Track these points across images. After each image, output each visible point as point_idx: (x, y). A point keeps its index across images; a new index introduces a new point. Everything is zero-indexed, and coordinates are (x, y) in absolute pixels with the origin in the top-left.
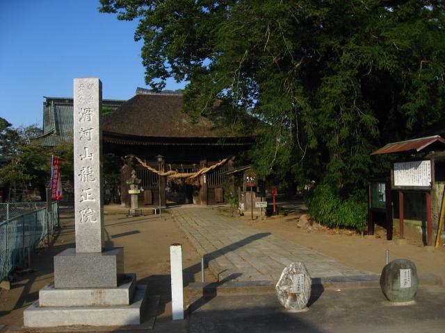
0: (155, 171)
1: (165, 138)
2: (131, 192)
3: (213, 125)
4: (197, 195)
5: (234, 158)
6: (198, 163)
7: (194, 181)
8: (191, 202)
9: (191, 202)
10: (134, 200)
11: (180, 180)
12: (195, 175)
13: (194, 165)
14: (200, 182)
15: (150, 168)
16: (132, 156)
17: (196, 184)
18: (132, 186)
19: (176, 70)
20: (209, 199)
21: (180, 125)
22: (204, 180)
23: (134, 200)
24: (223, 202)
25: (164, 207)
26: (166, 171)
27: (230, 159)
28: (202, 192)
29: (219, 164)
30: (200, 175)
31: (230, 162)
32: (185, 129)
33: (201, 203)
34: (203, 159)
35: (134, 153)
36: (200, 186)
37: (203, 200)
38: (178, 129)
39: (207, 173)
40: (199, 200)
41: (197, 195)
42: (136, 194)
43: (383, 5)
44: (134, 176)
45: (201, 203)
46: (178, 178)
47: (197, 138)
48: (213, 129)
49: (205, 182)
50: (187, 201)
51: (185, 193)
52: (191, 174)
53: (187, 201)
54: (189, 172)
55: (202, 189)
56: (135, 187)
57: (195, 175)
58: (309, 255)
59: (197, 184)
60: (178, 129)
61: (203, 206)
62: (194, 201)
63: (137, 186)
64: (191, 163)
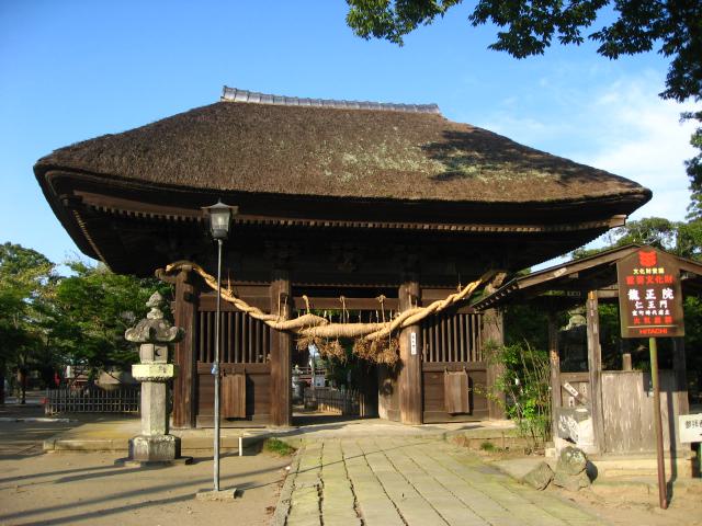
0: (257, 314)
1: (284, 195)
2: (139, 371)
3: (441, 168)
4: (390, 391)
5: (503, 276)
6: (393, 294)
7: (380, 349)
8: (374, 415)
9: (374, 415)
10: (151, 400)
11: (336, 345)
12: (385, 328)
13: (382, 297)
14: (398, 352)
15: (241, 306)
16: (186, 266)
17: (387, 357)
18: (146, 350)
19: (353, 381)
20: (427, 405)
21: (336, 166)
22: (409, 345)
23: (151, 400)
24: (470, 414)
25: (285, 428)
26: (293, 316)
27: (491, 280)
28: (406, 383)
29: (457, 297)
30: (399, 330)
31: (490, 289)
32: (350, 175)
33: (403, 415)
34: (408, 280)
35: (191, 259)
36: (399, 364)
37: (409, 405)
38: (328, 174)
39: (422, 324)
40: (394, 405)
41: (390, 391)
42: (156, 380)
43: (694, 31)
44: (154, 315)
45: (403, 415)
46: (332, 339)
47: (389, 200)
48: (439, 178)
49: (414, 351)
50: (362, 410)
51: (361, 384)
52: (370, 326)
53: (362, 410)
54: (365, 321)
55: (404, 374)
56: (156, 354)
57: (385, 328)
58: (443, 451)
59: (387, 360)
60: (328, 174)
61: (407, 426)
62: (382, 411)
63: (164, 351)
64: (373, 294)
